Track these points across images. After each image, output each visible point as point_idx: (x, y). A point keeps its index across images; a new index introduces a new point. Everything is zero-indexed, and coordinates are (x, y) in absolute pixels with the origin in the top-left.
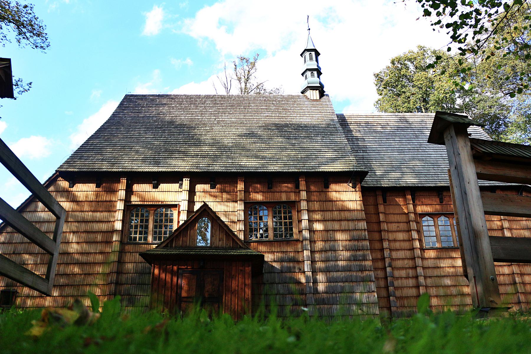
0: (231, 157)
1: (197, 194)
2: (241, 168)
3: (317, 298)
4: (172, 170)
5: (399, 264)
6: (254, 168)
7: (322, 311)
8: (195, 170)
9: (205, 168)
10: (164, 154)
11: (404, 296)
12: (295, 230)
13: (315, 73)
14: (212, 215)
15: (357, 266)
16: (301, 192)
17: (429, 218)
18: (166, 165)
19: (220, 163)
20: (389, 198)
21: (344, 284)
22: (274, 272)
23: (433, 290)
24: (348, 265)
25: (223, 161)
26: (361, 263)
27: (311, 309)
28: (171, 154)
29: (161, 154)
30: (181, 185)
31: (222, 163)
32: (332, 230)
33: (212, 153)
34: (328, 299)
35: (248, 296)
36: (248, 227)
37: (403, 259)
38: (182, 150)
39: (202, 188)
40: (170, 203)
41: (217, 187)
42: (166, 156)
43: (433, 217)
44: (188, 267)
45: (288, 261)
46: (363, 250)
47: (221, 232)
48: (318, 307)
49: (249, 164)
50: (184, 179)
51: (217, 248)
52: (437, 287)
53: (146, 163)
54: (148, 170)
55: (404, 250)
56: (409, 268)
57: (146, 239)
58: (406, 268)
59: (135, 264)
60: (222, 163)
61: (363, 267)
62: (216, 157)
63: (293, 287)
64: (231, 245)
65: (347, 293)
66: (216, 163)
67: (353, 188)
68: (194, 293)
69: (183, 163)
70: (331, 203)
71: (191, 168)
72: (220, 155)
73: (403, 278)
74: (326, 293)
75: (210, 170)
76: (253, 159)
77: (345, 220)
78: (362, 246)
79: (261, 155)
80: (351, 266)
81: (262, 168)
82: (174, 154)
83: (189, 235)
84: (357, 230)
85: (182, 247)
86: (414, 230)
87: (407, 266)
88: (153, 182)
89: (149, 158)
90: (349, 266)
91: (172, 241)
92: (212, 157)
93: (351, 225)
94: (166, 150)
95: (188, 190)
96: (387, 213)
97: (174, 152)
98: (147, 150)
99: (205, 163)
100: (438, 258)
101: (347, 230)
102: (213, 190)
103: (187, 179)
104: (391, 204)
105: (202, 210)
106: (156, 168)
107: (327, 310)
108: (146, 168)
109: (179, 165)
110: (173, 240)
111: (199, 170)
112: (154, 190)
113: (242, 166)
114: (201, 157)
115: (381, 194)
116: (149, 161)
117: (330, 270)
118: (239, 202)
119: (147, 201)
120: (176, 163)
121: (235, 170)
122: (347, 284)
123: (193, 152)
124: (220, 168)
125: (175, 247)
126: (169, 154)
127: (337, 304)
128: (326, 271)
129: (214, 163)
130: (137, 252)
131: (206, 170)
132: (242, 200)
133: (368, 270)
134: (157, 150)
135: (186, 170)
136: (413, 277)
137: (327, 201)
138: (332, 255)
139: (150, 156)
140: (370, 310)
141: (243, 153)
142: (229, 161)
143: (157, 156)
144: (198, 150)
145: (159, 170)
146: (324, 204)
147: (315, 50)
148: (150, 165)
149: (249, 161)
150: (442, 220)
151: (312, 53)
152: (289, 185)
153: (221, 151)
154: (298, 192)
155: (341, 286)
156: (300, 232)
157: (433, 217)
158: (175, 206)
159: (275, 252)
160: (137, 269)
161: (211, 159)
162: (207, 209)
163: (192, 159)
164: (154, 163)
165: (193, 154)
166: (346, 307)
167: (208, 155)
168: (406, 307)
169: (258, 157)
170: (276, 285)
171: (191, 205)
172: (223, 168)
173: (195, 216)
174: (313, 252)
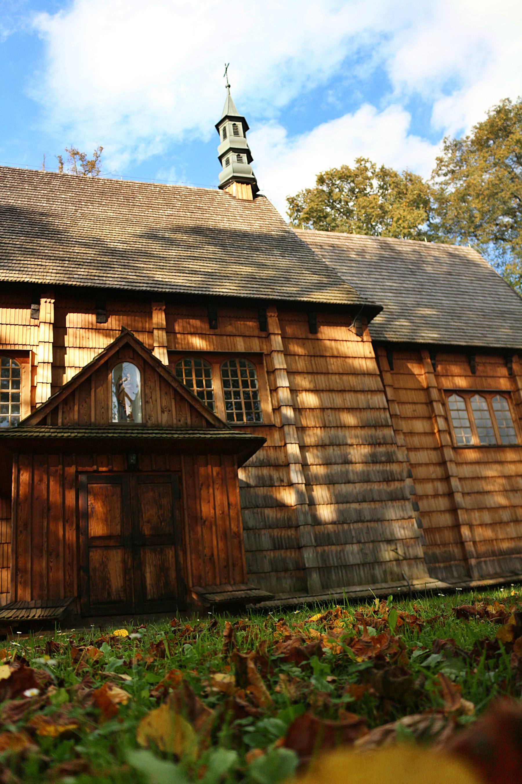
1: (69, 331)
3: (317, 532)
5: (421, 472)
7: (328, 557)
11: (434, 526)
12: (267, 406)
13: (244, 157)
14: (144, 355)
15: (378, 472)
16: (272, 337)
17: (459, 398)
20: (397, 363)
21: (361, 507)
23: (475, 514)
24: (363, 472)
26: (385, 468)
27: (311, 555)
32: (331, 409)
34: (337, 534)
37: (427, 464)
43: (463, 396)
45: (258, 464)
46: (385, 444)
48: (319, 549)
50: (43, 300)
51: (158, 427)
52: (481, 509)
55: (427, 449)
56: (437, 479)
58: (433, 480)
60: (116, 276)
61: (389, 474)
63: (270, 513)
64: (189, 421)
65: (368, 521)
67: (357, 335)
68: (119, 527)
70: (324, 358)
73: (430, 497)
74: (333, 523)
78: (384, 438)
80: (368, 472)
82: (13, 255)
84: (373, 408)
86: (440, 416)
87: (434, 476)
90: (366, 473)
93: (362, 400)
95: (52, 322)
96: (396, 386)
101: (356, 409)
103: (49, 300)
104: (401, 371)
105: (121, 344)
107: (336, 554)
115: (385, 355)
117: (334, 482)
122: (365, 505)
127: (353, 544)
128: (328, 482)
132: (163, 347)
133: (398, 480)
135: (47, 281)
136: (444, 495)
137: (317, 356)
138: (335, 453)
140: (408, 551)
146: (313, 362)
147: (242, 120)
150: (478, 401)
151: (237, 123)
152: (250, 324)
154: (265, 338)
155: (356, 510)
156: (277, 409)
157: (463, 396)
158: (24, 354)
166: (369, 547)
168: (439, 545)
171: (58, 354)
173: (106, 358)
174: (303, 448)
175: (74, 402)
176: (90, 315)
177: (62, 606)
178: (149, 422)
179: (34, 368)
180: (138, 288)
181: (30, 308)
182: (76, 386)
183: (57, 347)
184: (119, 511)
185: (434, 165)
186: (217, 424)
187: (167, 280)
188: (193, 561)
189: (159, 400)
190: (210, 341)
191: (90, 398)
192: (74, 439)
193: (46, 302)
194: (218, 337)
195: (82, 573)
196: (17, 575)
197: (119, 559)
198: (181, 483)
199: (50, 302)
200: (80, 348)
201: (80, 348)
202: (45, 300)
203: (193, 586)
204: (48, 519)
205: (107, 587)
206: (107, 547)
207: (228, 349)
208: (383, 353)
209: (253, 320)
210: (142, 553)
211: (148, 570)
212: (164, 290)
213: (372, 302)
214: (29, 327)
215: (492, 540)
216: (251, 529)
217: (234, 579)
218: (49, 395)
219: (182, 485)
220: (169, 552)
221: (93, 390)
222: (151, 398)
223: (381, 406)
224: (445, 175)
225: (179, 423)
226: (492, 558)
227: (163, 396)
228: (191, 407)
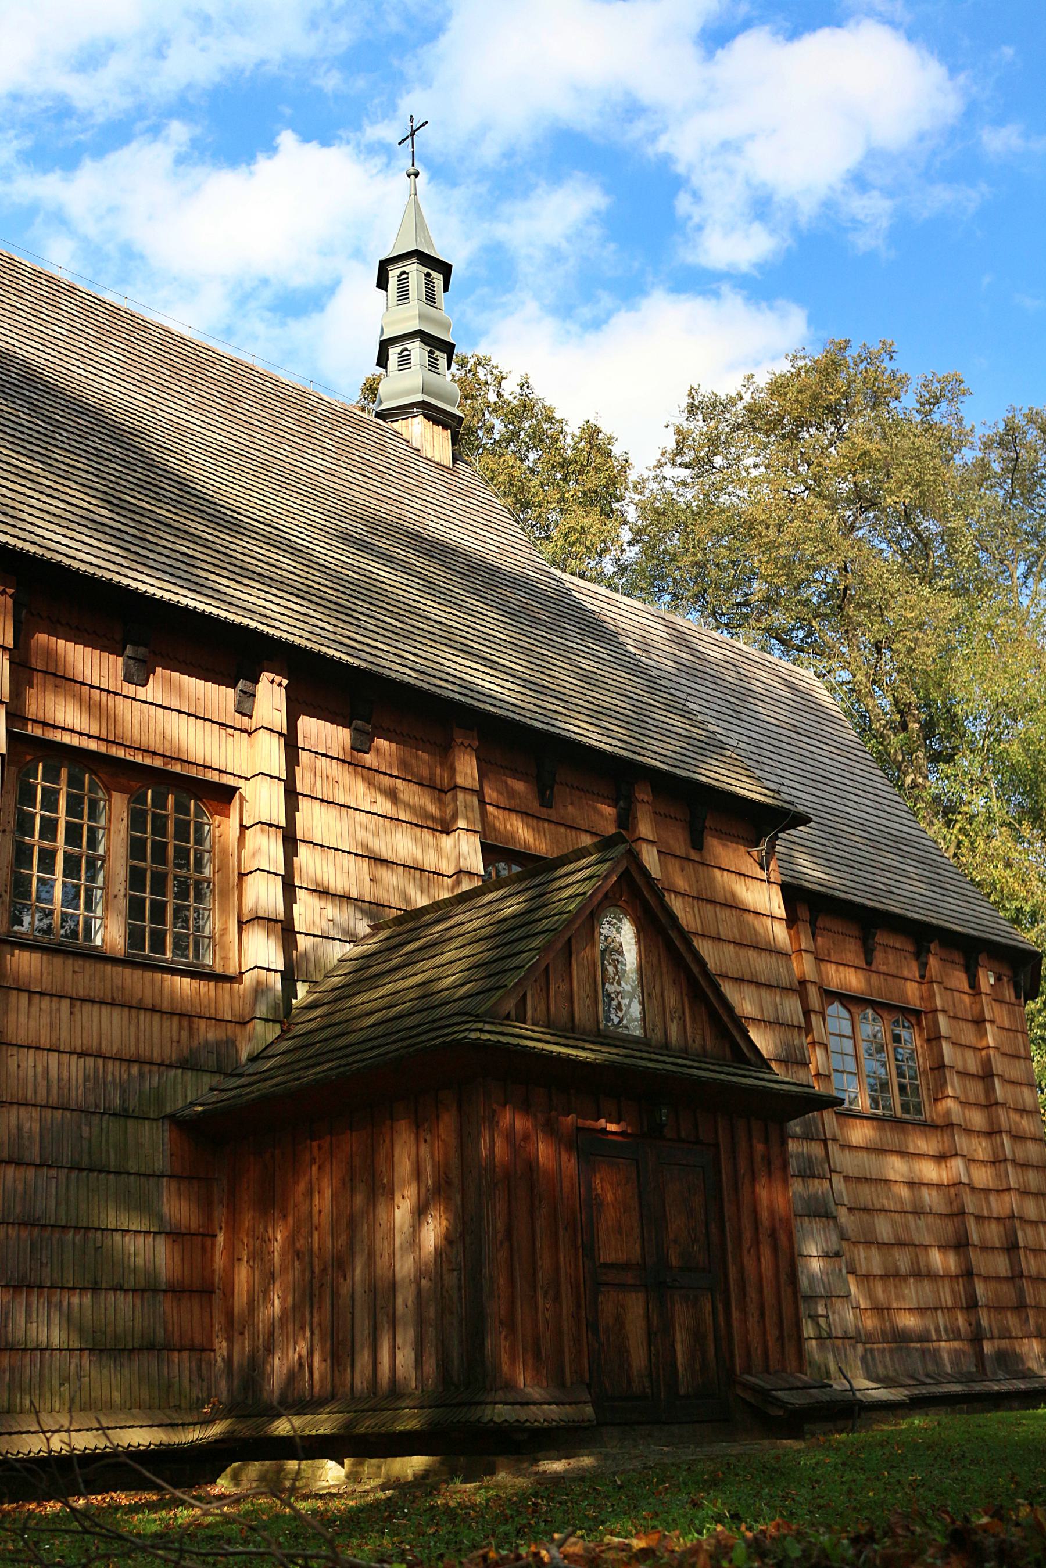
50: (265, 677)
54: (344, 657)
77: (752, 982)
100: (877, 1150)
103: (278, 679)
112: (130, 689)
147: (446, 269)
151: (434, 274)
176: (89, 649)
181: (234, 687)
185: (670, 442)
192: (584, 1064)
194: (553, 826)
200: (322, 800)
201: (322, 800)
202: (271, 676)
208: (804, 913)
209: (607, 801)
213: (791, 803)
214: (230, 731)
215: (882, 1309)
223: (795, 1024)
224: (687, 466)
226: (880, 1346)
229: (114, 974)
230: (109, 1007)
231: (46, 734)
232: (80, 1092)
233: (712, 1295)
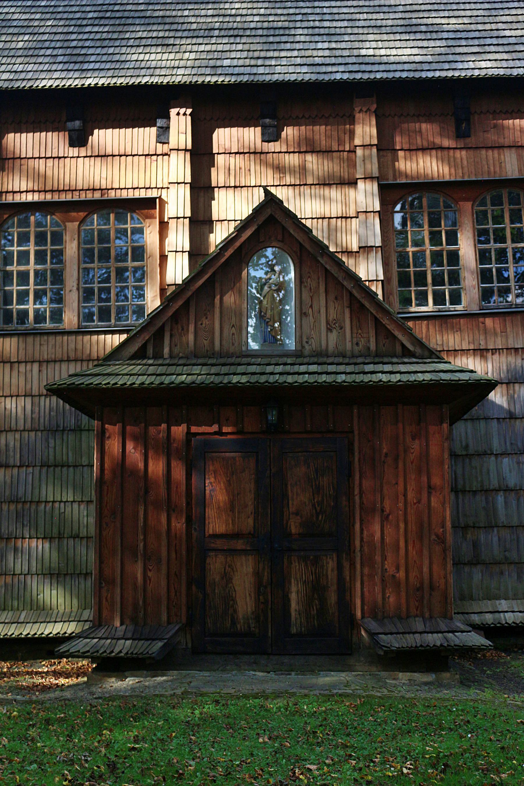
0: (322, 31)
1: (220, 160)
2: (363, 68)
4: (132, 81)
6: (406, 67)
8: (208, 79)
9: (242, 70)
10: (96, 29)
18: (108, 66)
19: (289, 54)
22: (486, 419)
25: (298, 46)
28: (120, 29)
29: (88, 29)
30: (164, 131)
31: (295, 53)
33: (257, 18)
35: (443, 526)
36: (395, 269)
38: (157, 14)
39: (235, 139)
40: (131, 194)
41: (284, 134)
42: (105, 36)
44: (225, 430)
47: (332, 297)
49: (388, 52)
50: (173, 112)
53: (40, 60)
57: (57, 316)
59: (29, 400)
60: (295, 53)
62: (272, 32)
64: (373, 346)
66: (276, 54)
68: (251, 521)
69: (165, 57)
71: (194, 71)
72: (286, 24)
75: (261, 78)
76: (398, 37)
79: (425, 21)
81: (434, 66)
82: (132, 28)
83: (217, 311)
85: (196, 356)
88: (70, 125)
89: (47, 44)
91: (159, 336)
92: (260, 32)
94: (101, 15)
95: (189, 147)
97: (130, 21)
98: (38, 16)
99: (238, 55)
102: (273, 146)
103: (182, 111)
105: (261, 219)
106: (77, 75)
108: (43, 75)
109: (153, 64)
110: (162, 329)
111: (221, 79)
112: (74, 152)
113: (367, 60)
114: (223, 33)
116: (49, 52)
118: (361, 184)
119: (52, 191)
120: (141, 57)
121: (345, 76)
123: (193, 20)
124: (291, 69)
125: (171, 357)
126: (111, 29)
129: (271, 54)
130: (33, 362)
131: (245, 78)
132: (372, 178)
134: (71, 16)
135: (179, 79)
139: (51, 37)
141: (361, 16)
142: (320, 45)
143: (74, 37)
144: (210, 12)
145: (88, 82)
148: (54, 67)
149: (386, 44)
153: (285, 12)
159: (487, 350)
160: (36, 416)
161: (258, 40)
162: (279, 216)
163: (194, 41)
164: (66, 59)
165: (194, 26)
167: (246, 26)
169: (414, 29)
170: (493, 458)
171: (202, 200)
172: (305, 69)
175: (188, 319)
177: (161, 639)
178: (307, 347)
179: (163, 226)
180: (327, 78)
181: (155, 125)
182: (189, 293)
183: (200, 188)
184: (253, 495)
186: (418, 351)
187: (383, 52)
188: (365, 578)
189: (323, 310)
190: (452, 163)
191: (214, 311)
193: (178, 114)
194: (471, 152)
195: (194, 588)
196: (100, 588)
197: (250, 570)
198: (351, 451)
199: (185, 114)
200: (235, 187)
203: (363, 617)
204: (145, 506)
205: (231, 611)
206: (233, 552)
207: (489, 173)
210: (285, 561)
211: (294, 589)
212: (372, 76)
214: (154, 158)
216: (512, 490)
217: (430, 610)
218: (186, 274)
219: (353, 454)
220: (328, 563)
221: (218, 297)
222: (311, 306)
225: (356, 348)
227: (331, 304)
228: (377, 322)
229: (70, 341)
230: (67, 363)
231: (15, 198)
232: (47, 419)
233: (338, 557)
